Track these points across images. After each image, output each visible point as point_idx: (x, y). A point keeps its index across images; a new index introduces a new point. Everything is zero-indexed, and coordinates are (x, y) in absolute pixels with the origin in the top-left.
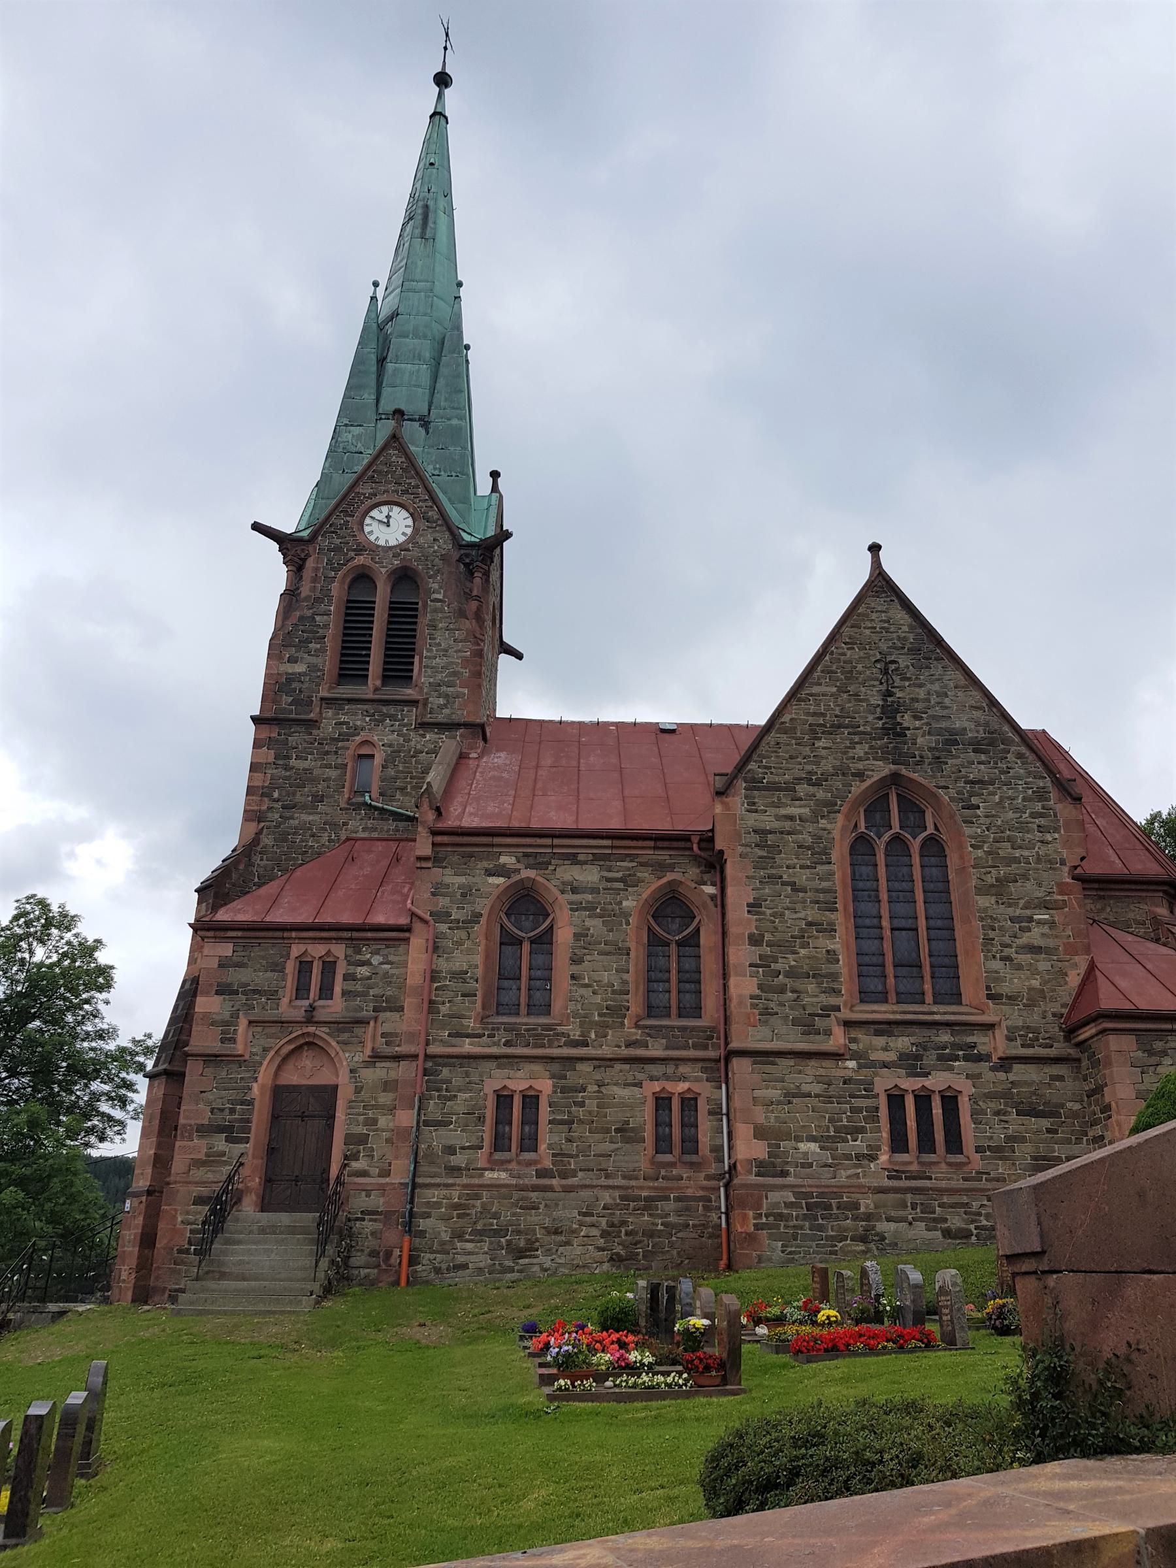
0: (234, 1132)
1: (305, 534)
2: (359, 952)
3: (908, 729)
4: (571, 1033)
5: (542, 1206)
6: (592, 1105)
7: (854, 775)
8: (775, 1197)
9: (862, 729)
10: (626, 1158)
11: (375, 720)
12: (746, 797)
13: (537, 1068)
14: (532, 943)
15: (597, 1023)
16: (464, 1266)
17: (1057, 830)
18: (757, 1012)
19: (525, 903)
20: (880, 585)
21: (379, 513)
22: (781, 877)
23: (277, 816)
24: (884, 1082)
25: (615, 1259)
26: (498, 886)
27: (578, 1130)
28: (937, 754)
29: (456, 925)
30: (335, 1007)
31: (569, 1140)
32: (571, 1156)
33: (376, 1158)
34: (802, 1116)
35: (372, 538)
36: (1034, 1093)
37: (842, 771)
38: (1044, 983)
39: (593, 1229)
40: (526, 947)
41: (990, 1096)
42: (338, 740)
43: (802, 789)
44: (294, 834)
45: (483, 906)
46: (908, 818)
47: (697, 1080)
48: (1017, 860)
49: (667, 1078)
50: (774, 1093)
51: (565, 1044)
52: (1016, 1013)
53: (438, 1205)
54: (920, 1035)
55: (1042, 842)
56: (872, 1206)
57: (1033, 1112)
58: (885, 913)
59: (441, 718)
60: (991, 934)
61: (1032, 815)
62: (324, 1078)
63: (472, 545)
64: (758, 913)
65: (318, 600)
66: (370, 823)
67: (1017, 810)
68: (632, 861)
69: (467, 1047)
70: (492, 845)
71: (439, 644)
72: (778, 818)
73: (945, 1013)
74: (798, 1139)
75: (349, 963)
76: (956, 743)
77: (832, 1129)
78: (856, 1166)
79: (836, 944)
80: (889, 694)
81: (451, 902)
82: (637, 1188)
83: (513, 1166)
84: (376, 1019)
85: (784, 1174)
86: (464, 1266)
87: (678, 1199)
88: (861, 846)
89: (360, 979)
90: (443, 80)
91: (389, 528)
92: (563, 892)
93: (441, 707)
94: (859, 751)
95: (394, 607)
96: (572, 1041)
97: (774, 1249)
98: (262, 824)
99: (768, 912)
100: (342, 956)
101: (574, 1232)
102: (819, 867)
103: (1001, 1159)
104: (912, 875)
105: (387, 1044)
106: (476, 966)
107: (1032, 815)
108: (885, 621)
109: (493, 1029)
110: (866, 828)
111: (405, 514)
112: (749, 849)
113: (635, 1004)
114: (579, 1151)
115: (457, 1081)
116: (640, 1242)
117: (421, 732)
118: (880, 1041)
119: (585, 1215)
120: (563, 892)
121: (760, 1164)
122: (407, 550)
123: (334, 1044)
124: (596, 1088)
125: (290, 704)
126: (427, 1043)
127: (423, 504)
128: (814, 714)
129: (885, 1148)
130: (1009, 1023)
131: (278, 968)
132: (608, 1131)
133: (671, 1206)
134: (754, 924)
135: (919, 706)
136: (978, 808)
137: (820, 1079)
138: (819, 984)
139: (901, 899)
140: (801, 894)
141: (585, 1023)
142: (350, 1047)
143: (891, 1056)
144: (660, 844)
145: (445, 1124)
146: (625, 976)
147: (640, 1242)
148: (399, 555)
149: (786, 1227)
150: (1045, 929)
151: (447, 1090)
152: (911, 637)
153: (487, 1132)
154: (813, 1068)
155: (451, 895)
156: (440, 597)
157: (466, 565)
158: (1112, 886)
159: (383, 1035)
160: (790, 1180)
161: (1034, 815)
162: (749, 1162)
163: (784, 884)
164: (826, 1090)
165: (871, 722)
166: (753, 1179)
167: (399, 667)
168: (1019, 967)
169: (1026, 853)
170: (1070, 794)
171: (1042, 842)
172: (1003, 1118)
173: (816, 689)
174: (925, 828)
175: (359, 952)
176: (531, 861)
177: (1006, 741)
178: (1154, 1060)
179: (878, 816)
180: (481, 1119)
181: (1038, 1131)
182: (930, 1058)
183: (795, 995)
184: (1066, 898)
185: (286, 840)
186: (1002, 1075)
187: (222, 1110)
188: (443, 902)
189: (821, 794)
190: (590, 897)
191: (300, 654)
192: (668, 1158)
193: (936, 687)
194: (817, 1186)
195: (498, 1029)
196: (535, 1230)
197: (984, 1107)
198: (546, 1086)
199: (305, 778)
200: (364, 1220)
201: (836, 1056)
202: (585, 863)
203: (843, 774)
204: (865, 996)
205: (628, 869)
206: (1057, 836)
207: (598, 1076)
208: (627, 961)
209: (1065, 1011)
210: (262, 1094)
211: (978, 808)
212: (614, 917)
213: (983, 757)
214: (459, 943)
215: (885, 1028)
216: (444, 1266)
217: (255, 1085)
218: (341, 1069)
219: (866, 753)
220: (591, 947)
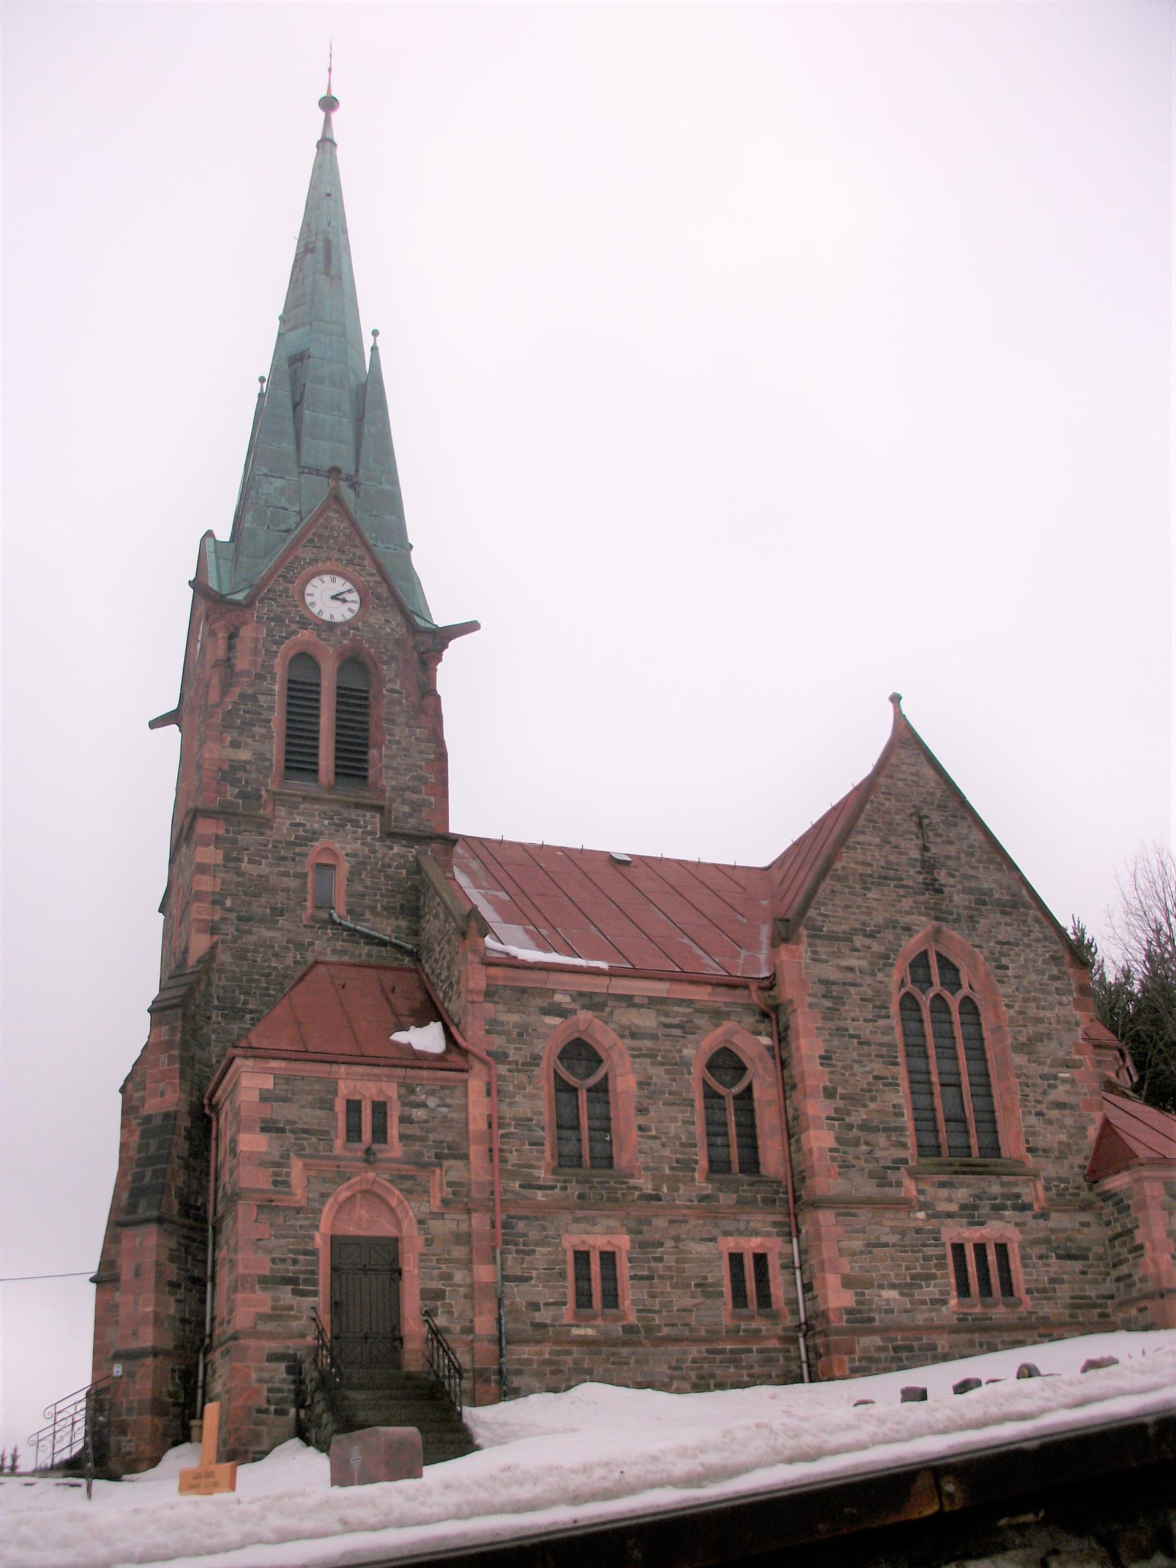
1: (240, 596)
4: (644, 1187)
5: (632, 1361)
6: (670, 1260)
11: (335, 824)
15: (668, 1176)
18: (836, 1164)
21: (341, 585)
22: (847, 1030)
23: (232, 929)
26: (555, 1026)
29: (516, 1068)
31: (653, 1296)
32: (654, 1312)
33: (456, 1315)
35: (315, 610)
37: (892, 924)
40: (583, 1096)
41: (1035, 1242)
42: (294, 844)
43: (859, 941)
47: (768, 1235)
48: (1040, 1021)
49: (741, 1233)
50: (857, 1244)
53: (529, 1362)
55: (1060, 1004)
56: (947, 1346)
57: (1069, 1257)
58: (933, 1068)
60: (1027, 1091)
62: (384, 1228)
64: (829, 1065)
65: (260, 677)
66: (339, 945)
68: (688, 1006)
71: (399, 742)
74: (881, 1287)
75: (404, 1104)
76: (984, 903)
78: (931, 1310)
80: (925, 849)
81: (509, 1042)
88: (909, 1004)
89: (418, 1122)
90: (329, 104)
91: (329, 598)
95: (343, 694)
98: (216, 937)
100: (395, 1096)
103: (1045, 1298)
104: (952, 1032)
106: (541, 1113)
109: (565, 1181)
114: (662, 1305)
115: (534, 1234)
117: (388, 843)
118: (944, 1193)
119: (675, 1369)
121: (849, 1311)
122: (357, 629)
124: (672, 1243)
125: (236, 797)
127: (372, 579)
128: (863, 864)
129: (954, 1293)
134: (827, 1077)
135: (951, 863)
138: (888, 1137)
143: (953, 1208)
145: (527, 1279)
146: (691, 1128)
148: (348, 633)
150: (1067, 1087)
151: (524, 1245)
152: (939, 793)
154: (890, 1219)
155: (507, 1033)
156: (397, 687)
161: (1053, 978)
162: (839, 1309)
163: (851, 1036)
164: (902, 1240)
165: (913, 877)
168: (1050, 1122)
173: (861, 838)
176: (586, 1001)
177: (1026, 906)
180: (562, 1275)
183: (869, 1148)
185: (246, 959)
186: (1041, 1222)
187: (284, 1260)
190: (648, 1043)
191: (243, 739)
195: (570, 1181)
198: (622, 1242)
199: (261, 887)
205: (684, 1015)
208: (692, 1113)
209: (1087, 1163)
211: (1007, 968)
212: (678, 1066)
213: (1008, 919)
217: (318, 1237)
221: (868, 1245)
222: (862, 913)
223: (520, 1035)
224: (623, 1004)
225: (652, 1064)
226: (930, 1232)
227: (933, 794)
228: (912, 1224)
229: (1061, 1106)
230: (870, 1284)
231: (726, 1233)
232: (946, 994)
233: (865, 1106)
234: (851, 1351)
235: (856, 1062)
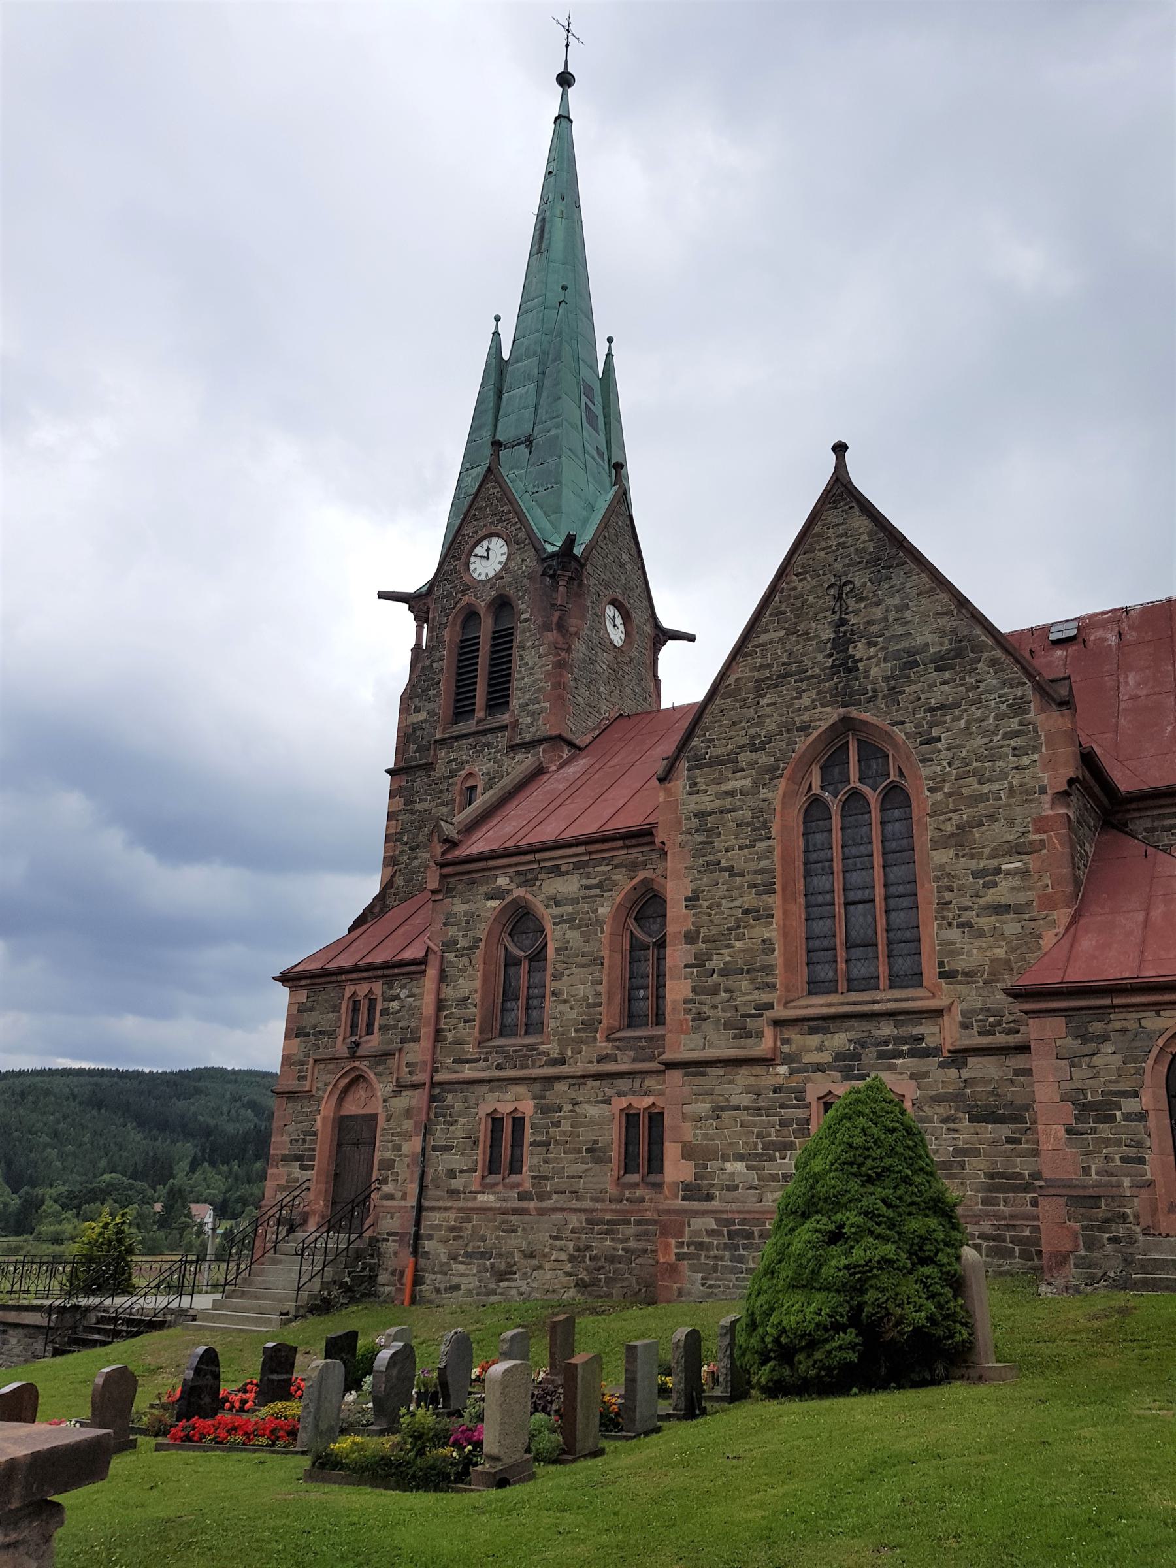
0: (303, 1160)
2: (391, 988)
3: (861, 660)
6: (566, 1125)
7: (799, 729)
8: (697, 1223)
9: (810, 673)
10: (595, 1180)
11: (477, 752)
12: (688, 778)
13: (521, 1089)
14: (530, 961)
15: (573, 1040)
16: (457, 1288)
17: (1036, 749)
18: (689, 1017)
19: (520, 920)
20: (841, 493)
22: (719, 863)
24: (816, 1087)
25: (581, 1285)
27: (556, 1152)
28: (893, 683)
30: (373, 1042)
31: (546, 1162)
32: (547, 1178)
34: (731, 1133)
36: (991, 1093)
37: (787, 728)
38: (1012, 950)
39: (562, 1253)
40: (525, 965)
41: (937, 1099)
42: (449, 778)
43: (744, 758)
44: (418, 872)
45: (482, 930)
46: (869, 767)
48: (984, 798)
49: (633, 1092)
50: (704, 1108)
51: (546, 1064)
52: (974, 992)
53: (438, 1227)
54: (858, 1030)
55: (1017, 768)
59: (528, 737)
60: (948, 896)
61: (1006, 737)
63: (553, 556)
67: (985, 733)
69: (467, 1072)
70: (490, 869)
71: (527, 664)
72: (719, 796)
73: (889, 1001)
74: (725, 1158)
76: (915, 664)
77: (760, 1146)
79: (771, 932)
80: (842, 622)
82: (601, 1210)
83: (500, 1189)
84: (400, 1050)
85: (709, 1198)
86: (457, 1288)
87: (638, 1223)
88: (815, 809)
90: (565, 80)
92: (547, 907)
93: (529, 725)
94: (806, 701)
96: (552, 1059)
97: (693, 1281)
99: (705, 904)
101: (545, 1256)
102: (758, 845)
105: (410, 1073)
107: (1006, 737)
108: (842, 536)
110: (861, 780)
111: (501, 542)
112: (689, 837)
113: (608, 1016)
115: (459, 1106)
116: (603, 1267)
118: (814, 1040)
119: (556, 1238)
120: (547, 907)
121: (687, 1187)
123: (372, 1076)
124: (570, 1107)
126: (435, 1070)
130: (965, 1006)
131: (335, 1009)
132: (579, 1152)
133: (630, 1230)
134: (691, 919)
136: (939, 740)
137: (751, 1088)
139: (859, 866)
140: (738, 879)
141: (563, 1042)
142: (384, 1078)
143: (826, 1058)
144: (628, 842)
145: (448, 1148)
146: (599, 988)
147: (603, 1267)
149: (707, 1257)
150: (1016, 881)
152: (870, 546)
153: (480, 1155)
154: (745, 1076)
156: (527, 616)
157: (551, 576)
158: (1162, 802)
159: (408, 1065)
160: (715, 1204)
164: (755, 1101)
165: (819, 660)
166: (679, 1203)
167: (499, 699)
168: (981, 934)
169: (996, 786)
170: (1054, 700)
171: (1017, 768)
172: (952, 1126)
173: (764, 638)
174: (848, 781)
175: (391, 988)
177: (978, 648)
178: (1090, 1047)
179: (836, 770)
180: (476, 1143)
181: (993, 1142)
182: (869, 1057)
183: (728, 995)
184: (1044, 836)
186: (953, 1073)
187: (297, 1141)
188: (452, 931)
189: (764, 759)
192: (635, 1178)
193: (896, 600)
194: (739, 1212)
196: (512, 1254)
197: (930, 1114)
200: (388, 1240)
201: (766, 1062)
202: (567, 873)
203: (788, 731)
204: (815, 987)
205: (604, 873)
206: (1036, 757)
207: (573, 1094)
208: (601, 972)
210: (324, 1124)
213: (947, 675)
214: (463, 970)
215: (820, 1024)
216: (442, 1286)
217: (319, 1118)
218: (378, 1098)
219: (814, 701)
220: (570, 961)
221: (714, 1109)
222: (753, 726)
223: (468, 922)
224: (551, 875)
225: (570, 928)
226: (792, 1090)
227: (864, 550)
228: (772, 1080)
229: (1001, 909)
230: (713, 1154)
231: (620, 1094)
232: (866, 789)
233: (730, 947)
234: (681, 1234)
235: (725, 898)
